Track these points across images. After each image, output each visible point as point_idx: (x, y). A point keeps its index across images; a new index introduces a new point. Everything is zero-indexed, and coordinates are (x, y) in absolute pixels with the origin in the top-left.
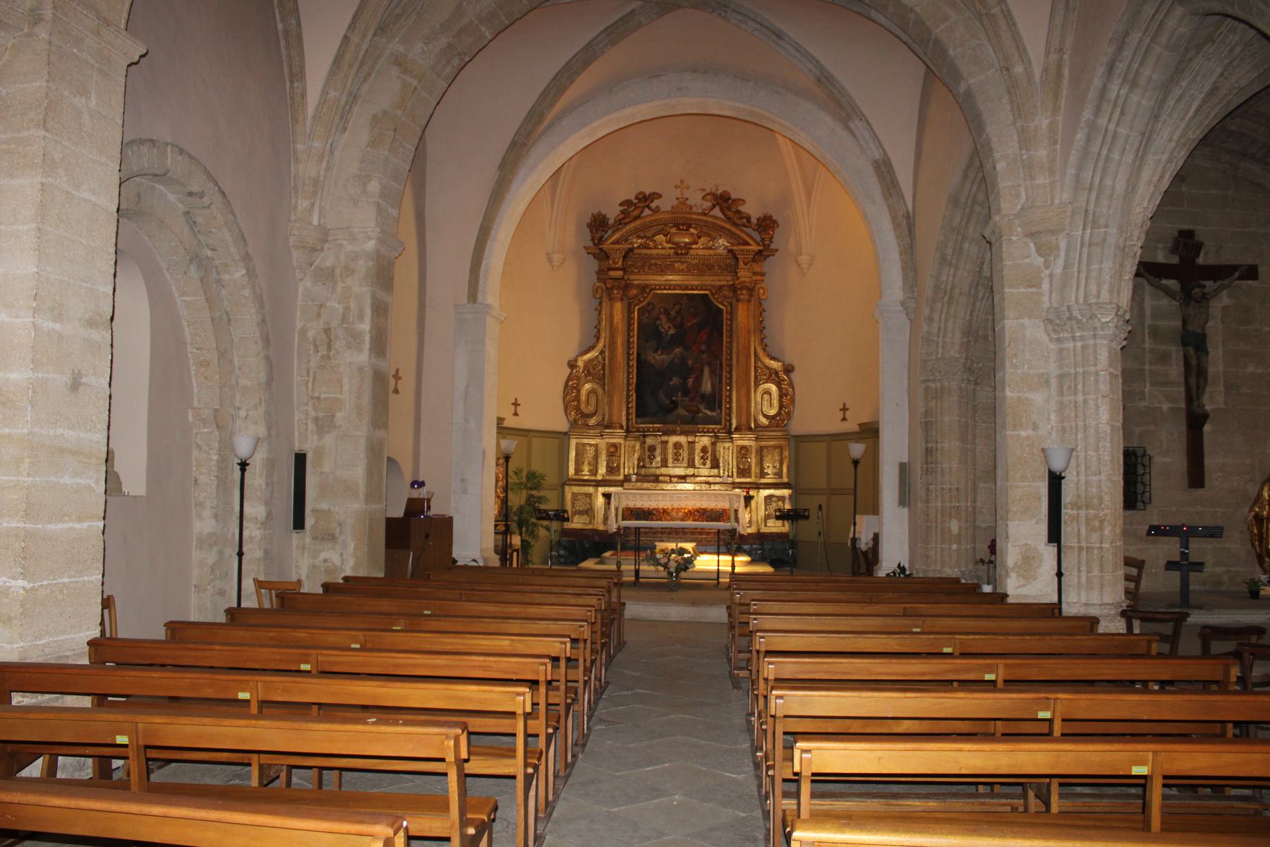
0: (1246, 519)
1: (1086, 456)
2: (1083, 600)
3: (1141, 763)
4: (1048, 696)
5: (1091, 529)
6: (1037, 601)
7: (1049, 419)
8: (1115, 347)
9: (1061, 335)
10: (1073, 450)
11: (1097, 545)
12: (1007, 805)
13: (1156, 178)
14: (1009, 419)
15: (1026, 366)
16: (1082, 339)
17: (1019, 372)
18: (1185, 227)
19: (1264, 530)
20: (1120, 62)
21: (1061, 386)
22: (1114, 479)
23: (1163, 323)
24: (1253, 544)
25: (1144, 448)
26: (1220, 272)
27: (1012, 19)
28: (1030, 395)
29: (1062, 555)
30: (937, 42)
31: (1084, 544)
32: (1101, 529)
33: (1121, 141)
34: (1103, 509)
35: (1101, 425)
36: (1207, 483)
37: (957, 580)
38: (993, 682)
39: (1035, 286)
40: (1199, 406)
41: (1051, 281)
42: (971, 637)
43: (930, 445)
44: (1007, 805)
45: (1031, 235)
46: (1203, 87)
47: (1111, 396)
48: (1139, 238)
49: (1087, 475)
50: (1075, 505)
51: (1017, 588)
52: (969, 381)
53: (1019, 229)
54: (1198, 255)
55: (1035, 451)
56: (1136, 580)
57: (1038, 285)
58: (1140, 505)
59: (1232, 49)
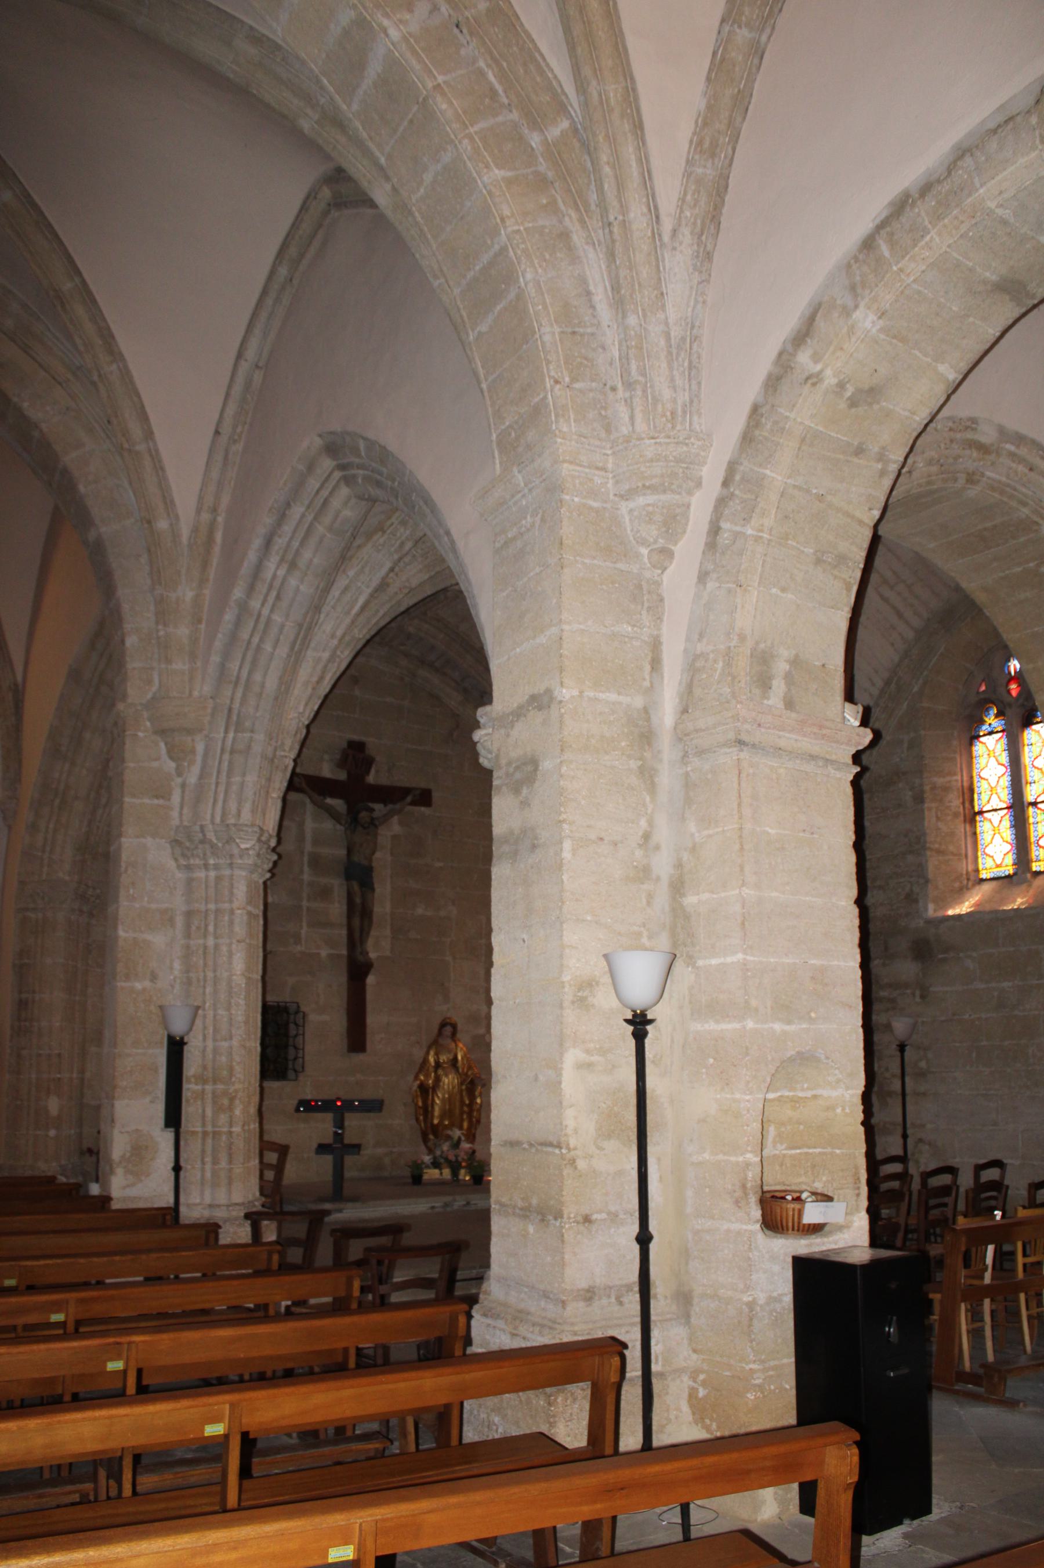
0: (411, 1089)
1: (215, 1016)
2: (208, 1200)
3: (215, 1420)
4: (118, 1340)
5: (218, 1109)
6: (148, 1205)
7: (171, 968)
8: (256, 879)
9: (192, 861)
10: (198, 1008)
11: (225, 1129)
12: (74, 1492)
13: (315, 679)
14: (120, 967)
15: (146, 899)
16: (216, 867)
17: (137, 905)
18: (356, 737)
19: (430, 1102)
20: (280, 536)
21: (188, 926)
22: (248, 1044)
23: (326, 851)
24: (417, 1120)
25: (297, 1003)
26: (392, 795)
27: (160, 461)
28: (148, 937)
29: (182, 1143)
30: (65, 472)
31: (209, 1128)
32: (231, 1108)
33: (274, 631)
34: (233, 1084)
35: (234, 977)
36: (369, 1045)
37: (52, 1179)
38: (63, 1325)
39: (163, 797)
40: (361, 953)
41: (183, 792)
42: (42, 1262)
43: (24, 996)
44: (74, 1492)
45: (162, 732)
46: (370, 580)
47: (248, 941)
48: (291, 749)
49: (215, 1040)
50: (202, 1079)
51: (124, 1188)
52: (81, 911)
53: (148, 724)
54: (368, 772)
55: (152, 1008)
56: (279, 1168)
57: (166, 796)
58: (291, 1074)
59: (402, 544)
